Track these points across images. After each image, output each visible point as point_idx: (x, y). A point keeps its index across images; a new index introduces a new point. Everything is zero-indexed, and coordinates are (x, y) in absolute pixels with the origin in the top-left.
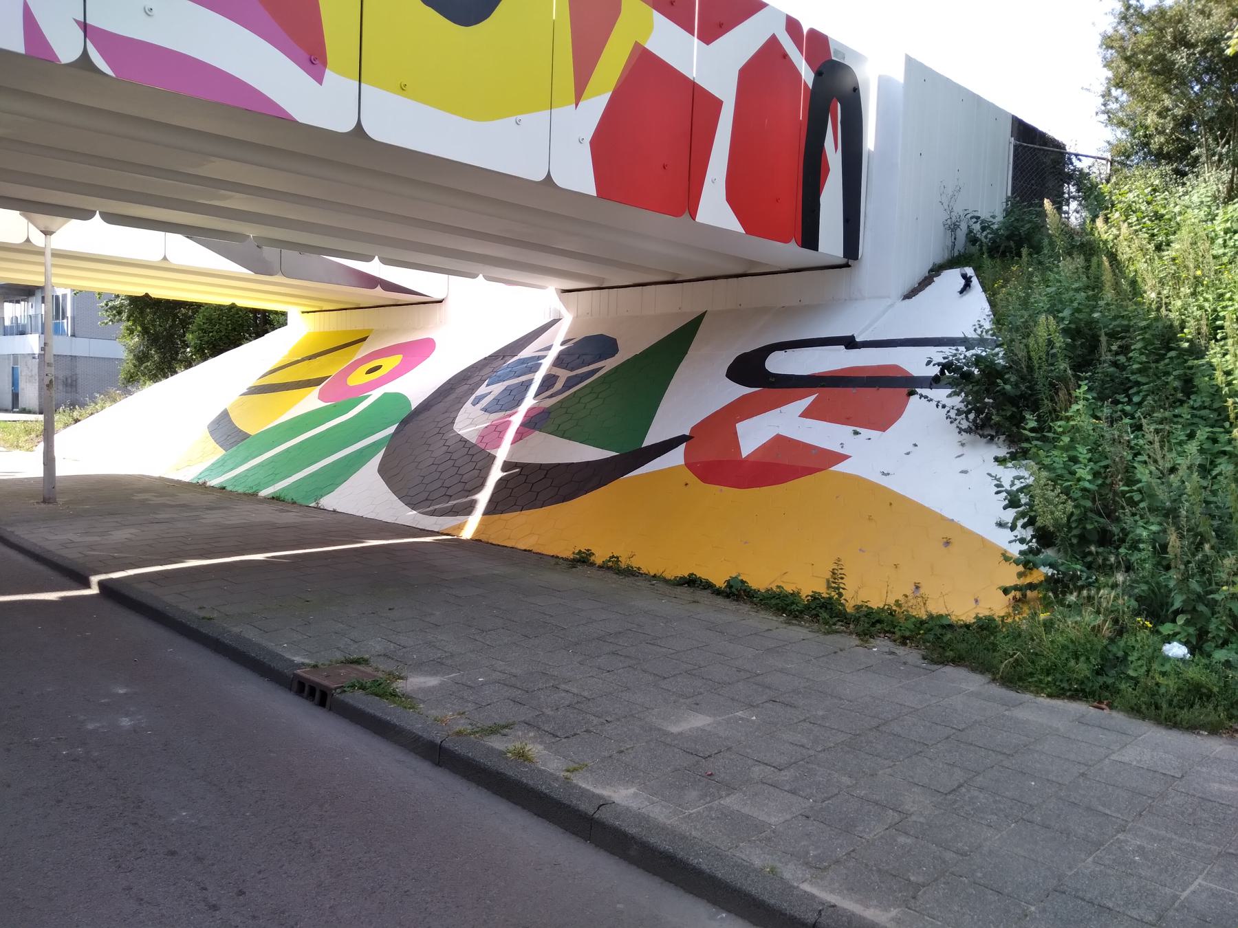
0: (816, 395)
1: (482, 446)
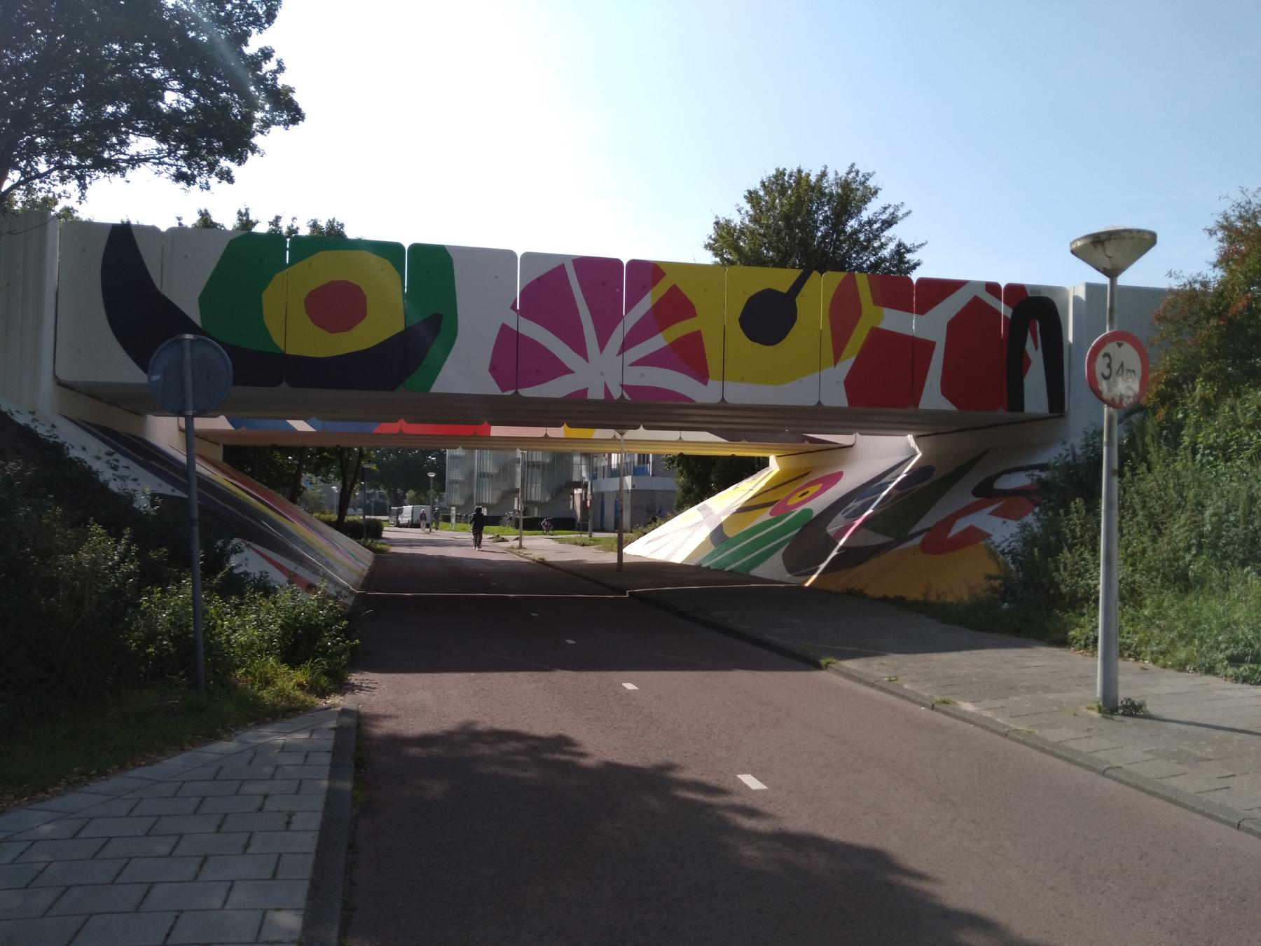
0: (1000, 504)
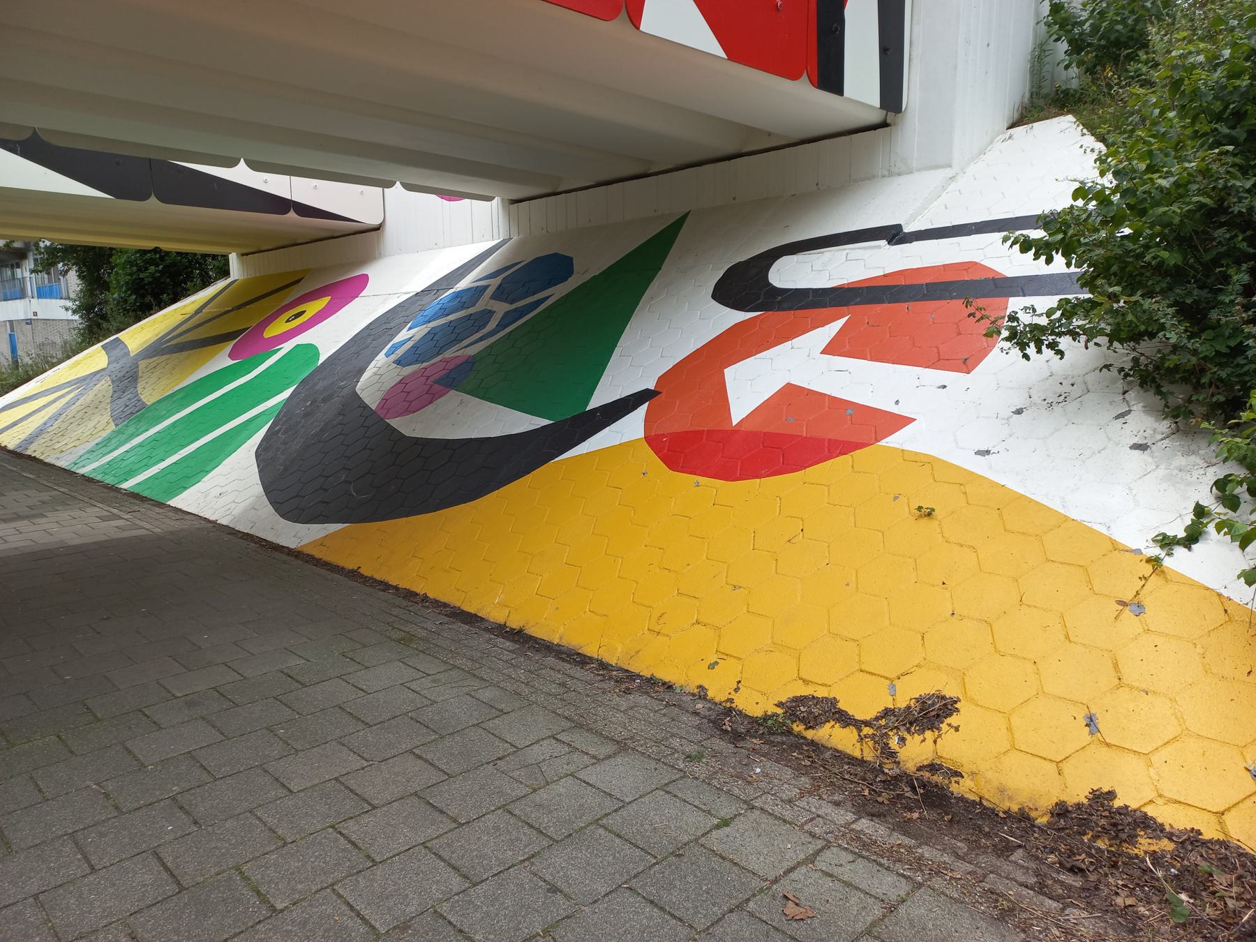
1: (381, 413)
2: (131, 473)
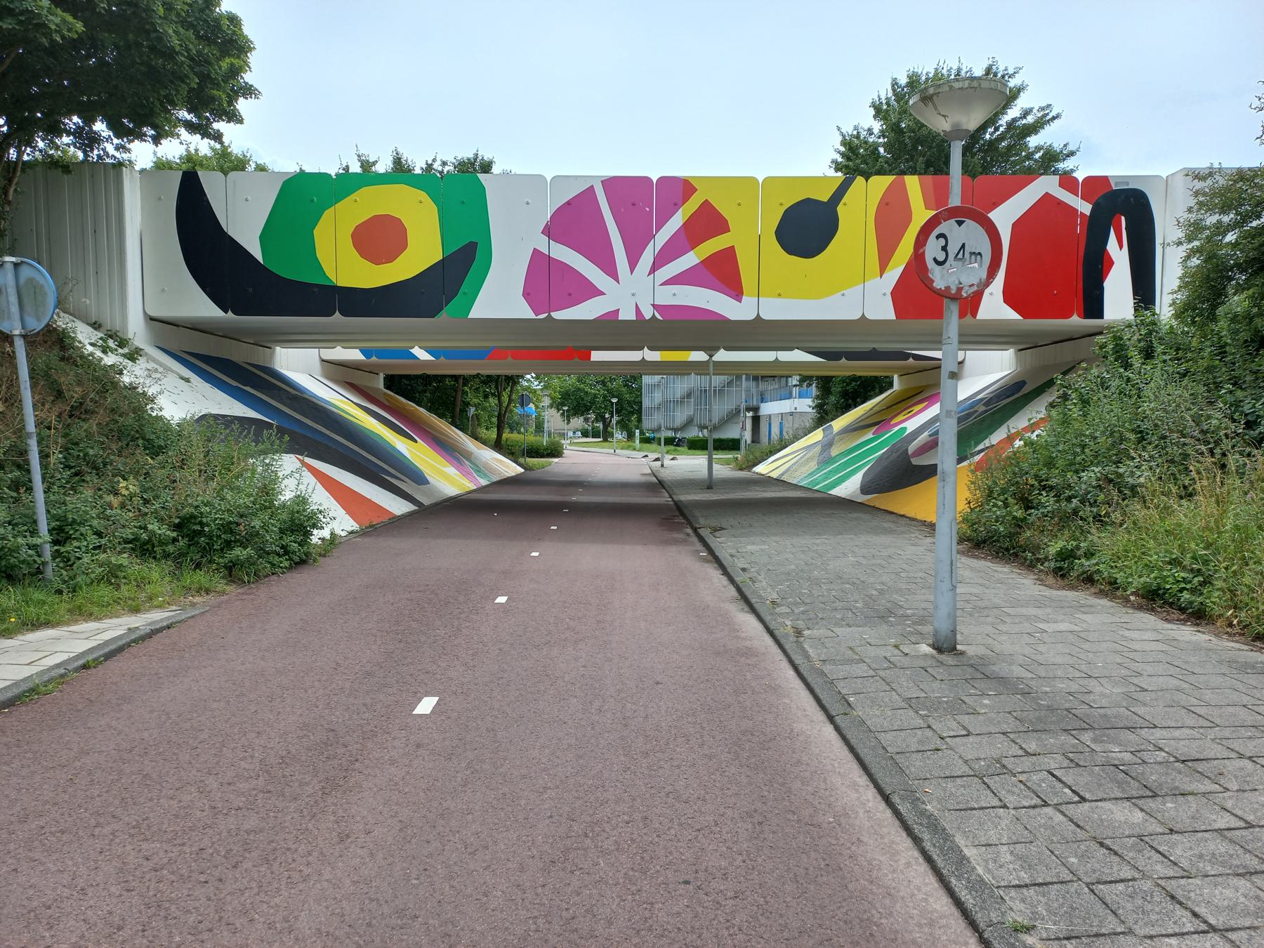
2: (818, 484)
